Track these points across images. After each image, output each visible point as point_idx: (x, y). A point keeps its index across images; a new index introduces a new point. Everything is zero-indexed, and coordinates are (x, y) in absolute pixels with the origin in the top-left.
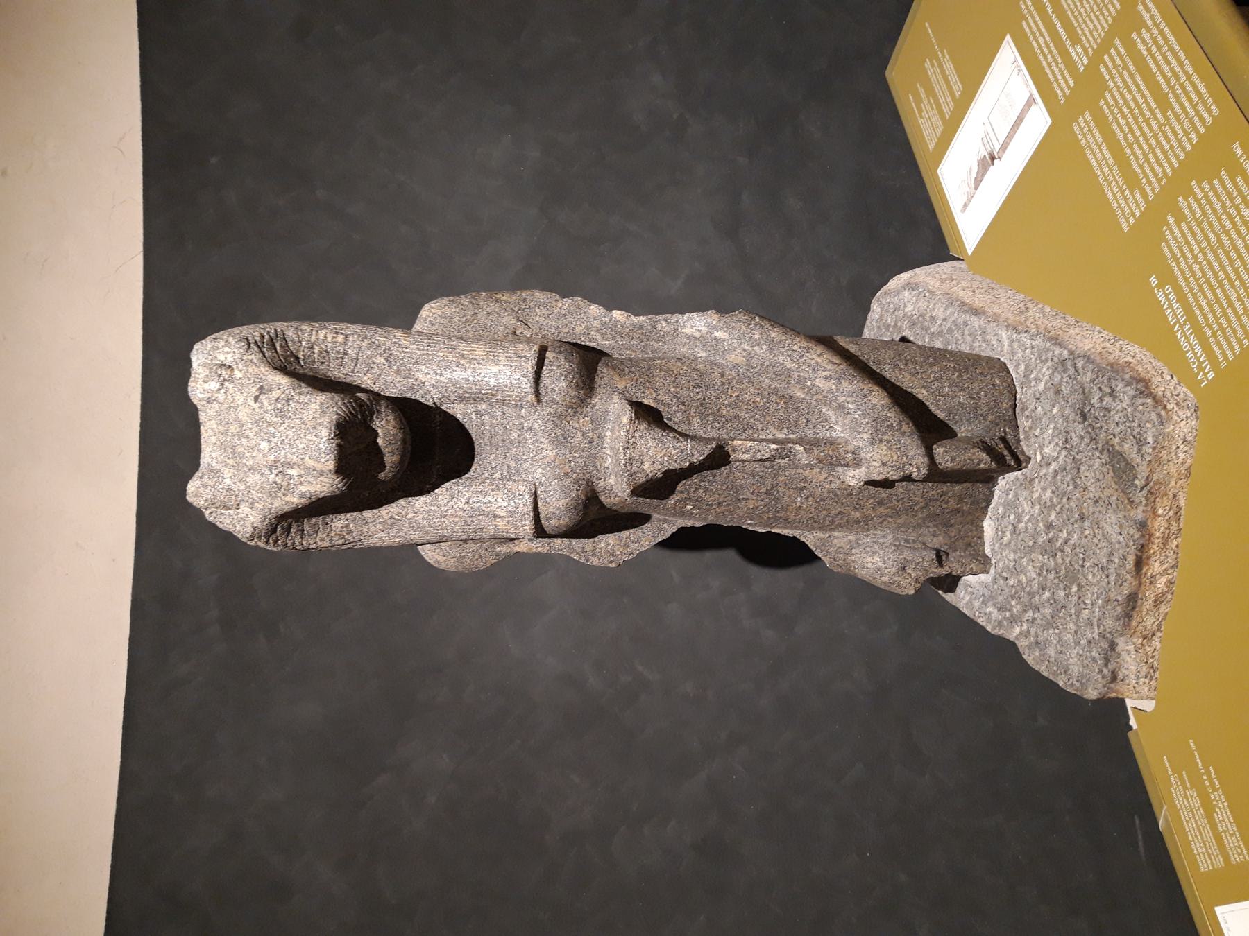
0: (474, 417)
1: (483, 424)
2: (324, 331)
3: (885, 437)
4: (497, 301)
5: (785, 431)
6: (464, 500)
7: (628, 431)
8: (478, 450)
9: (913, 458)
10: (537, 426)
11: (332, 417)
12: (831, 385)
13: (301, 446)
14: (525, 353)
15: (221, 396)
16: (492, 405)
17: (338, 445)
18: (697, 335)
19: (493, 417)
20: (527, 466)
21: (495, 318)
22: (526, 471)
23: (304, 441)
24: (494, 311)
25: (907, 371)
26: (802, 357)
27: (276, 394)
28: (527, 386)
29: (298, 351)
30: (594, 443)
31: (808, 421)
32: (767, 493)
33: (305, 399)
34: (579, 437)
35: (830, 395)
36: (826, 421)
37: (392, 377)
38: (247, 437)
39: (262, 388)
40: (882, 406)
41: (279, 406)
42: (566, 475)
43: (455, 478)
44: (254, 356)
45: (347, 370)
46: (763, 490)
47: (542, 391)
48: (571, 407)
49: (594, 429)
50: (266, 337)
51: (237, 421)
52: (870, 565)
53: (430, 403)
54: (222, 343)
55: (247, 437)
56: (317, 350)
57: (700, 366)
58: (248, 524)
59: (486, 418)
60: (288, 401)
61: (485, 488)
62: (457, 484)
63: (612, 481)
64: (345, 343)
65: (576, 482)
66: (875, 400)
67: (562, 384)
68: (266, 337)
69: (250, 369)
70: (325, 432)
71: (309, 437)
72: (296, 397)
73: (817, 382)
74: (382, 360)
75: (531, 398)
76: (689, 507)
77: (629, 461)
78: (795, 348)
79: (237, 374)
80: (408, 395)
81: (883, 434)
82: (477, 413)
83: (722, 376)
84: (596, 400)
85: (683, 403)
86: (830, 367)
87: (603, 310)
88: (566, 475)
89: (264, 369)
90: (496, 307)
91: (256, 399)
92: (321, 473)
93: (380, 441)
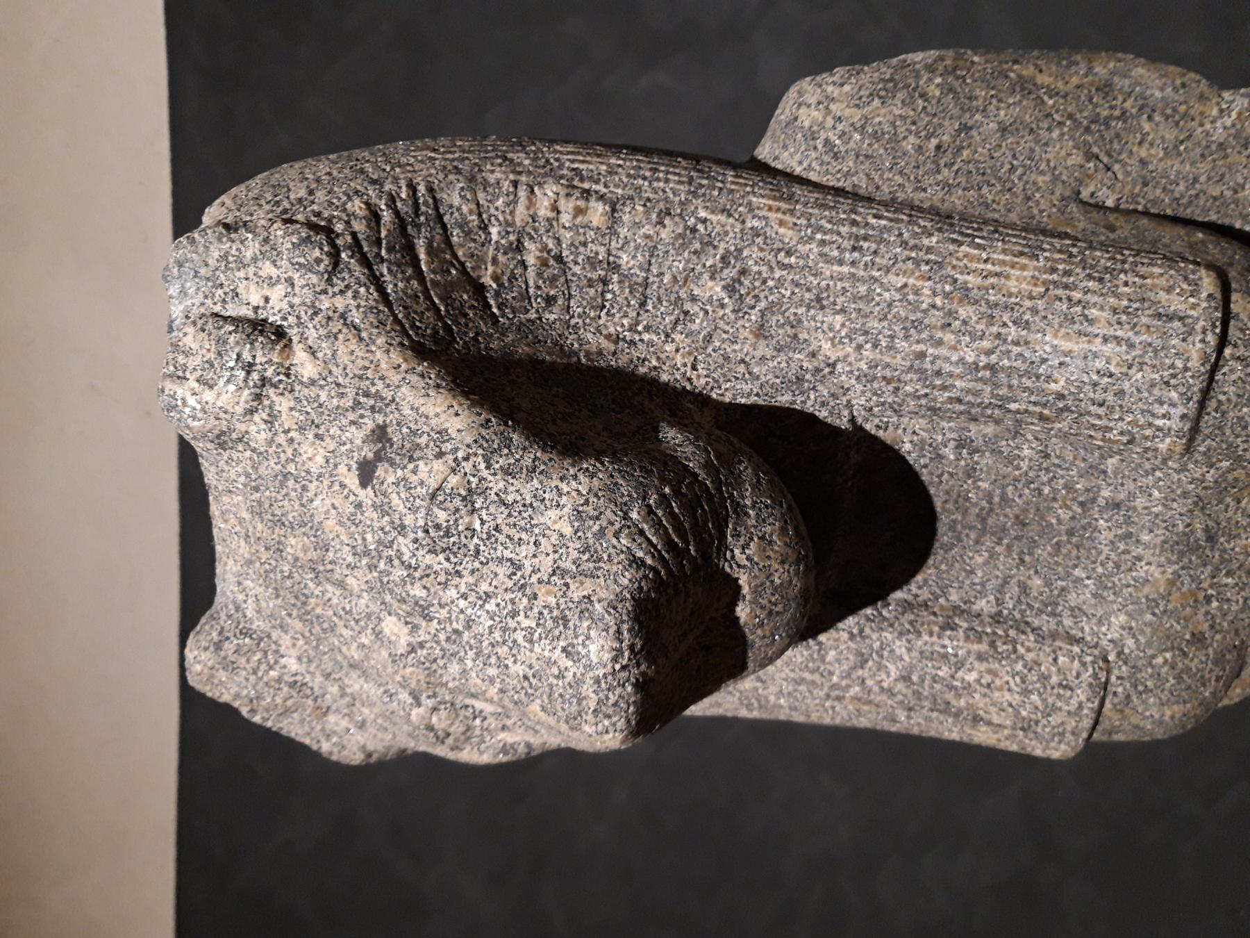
0: (949, 453)
2: (551, 189)
4: (1025, 87)
8: (944, 535)
13: (519, 669)
14: (1176, 304)
15: (257, 431)
20: (1082, 596)
21: (1027, 142)
22: (1076, 611)
24: (1028, 124)
27: (430, 472)
29: (480, 261)
37: (747, 346)
38: (341, 584)
39: (380, 434)
42: (1198, 639)
43: (871, 601)
44: (353, 301)
45: (616, 324)
50: (387, 216)
51: (305, 523)
53: (844, 423)
54: (252, 247)
55: (341, 584)
59: (987, 460)
62: (882, 623)
68: (387, 216)
71: (542, 648)
74: (718, 290)
80: (784, 399)
88: (1198, 639)
89: (388, 360)
91: (366, 473)
93: (743, 612)
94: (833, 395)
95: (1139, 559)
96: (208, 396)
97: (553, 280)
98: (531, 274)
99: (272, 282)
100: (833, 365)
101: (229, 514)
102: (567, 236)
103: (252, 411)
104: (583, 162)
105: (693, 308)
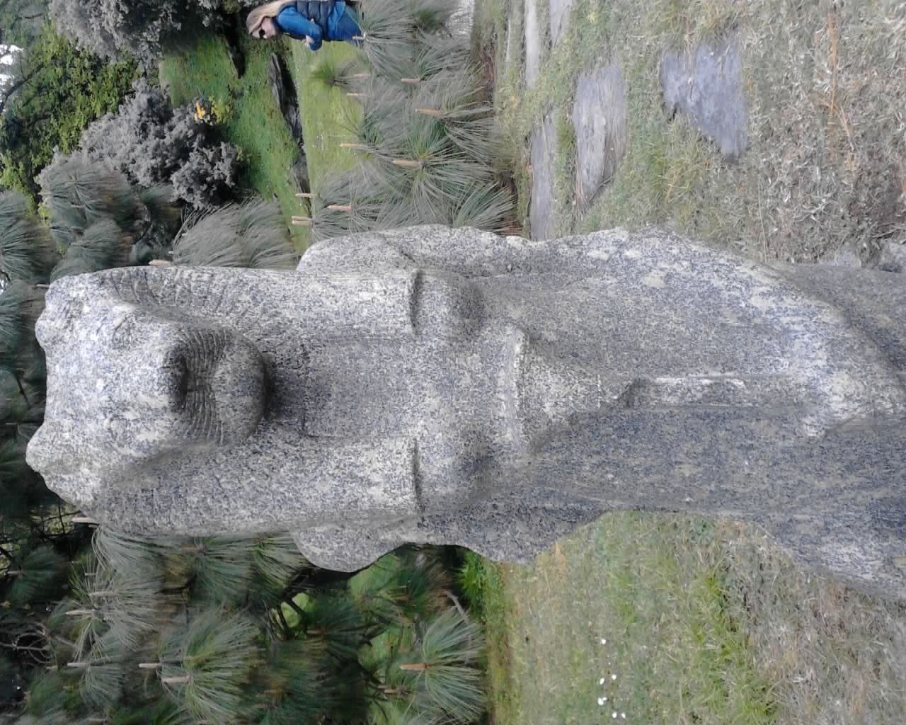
1: (358, 369)
3: (846, 363)
5: (720, 367)
6: (334, 464)
7: (522, 362)
9: (884, 388)
10: (417, 368)
11: (172, 343)
12: (770, 303)
13: (135, 379)
16: (366, 345)
17: (174, 375)
18: (605, 257)
19: (369, 360)
23: (139, 372)
25: (862, 293)
26: (731, 271)
28: (404, 316)
30: (485, 388)
31: (747, 354)
32: (705, 453)
33: (147, 326)
34: (466, 380)
35: (770, 317)
36: (769, 353)
40: (837, 326)
41: (118, 335)
46: (700, 450)
47: (421, 319)
48: (456, 339)
49: (484, 369)
52: (846, 559)
56: (179, 288)
57: (611, 294)
58: (88, 491)
59: (361, 362)
60: (128, 330)
61: (359, 447)
63: (509, 436)
64: (210, 282)
65: (464, 435)
66: (826, 319)
67: (445, 309)
69: (99, 303)
70: (159, 359)
72: (138, 325)
73: (753, 301)
75: (408, 329)
76: (610, 476)
77: (525, 402)
78: (722, 261)
79: (86, 309)
81: (843, 359)
82: (351, 357)
83: (638, 303)
84: (486, 332)
85: (591, 335)
86: (766, 281)
87: (495, 237)
88: (453, 426)
90: (378, 242)
92: (157, 413)
94: (293, 334)
95: (425, 395)
96: (53, 323)
97: (185, 296)
98: (177, 295)
99: (80, 289)
100: (291, 322)
101: (61, 195)
102: (193, 284)
103: (66, 327)
104: (445, 658)
105: (238, 304)
